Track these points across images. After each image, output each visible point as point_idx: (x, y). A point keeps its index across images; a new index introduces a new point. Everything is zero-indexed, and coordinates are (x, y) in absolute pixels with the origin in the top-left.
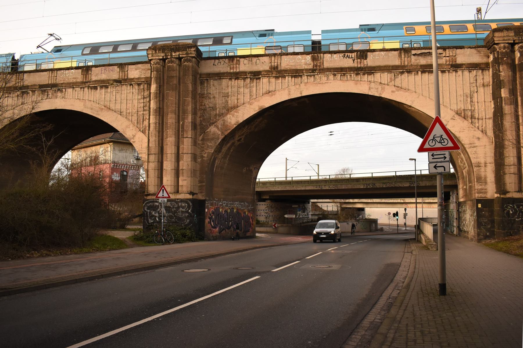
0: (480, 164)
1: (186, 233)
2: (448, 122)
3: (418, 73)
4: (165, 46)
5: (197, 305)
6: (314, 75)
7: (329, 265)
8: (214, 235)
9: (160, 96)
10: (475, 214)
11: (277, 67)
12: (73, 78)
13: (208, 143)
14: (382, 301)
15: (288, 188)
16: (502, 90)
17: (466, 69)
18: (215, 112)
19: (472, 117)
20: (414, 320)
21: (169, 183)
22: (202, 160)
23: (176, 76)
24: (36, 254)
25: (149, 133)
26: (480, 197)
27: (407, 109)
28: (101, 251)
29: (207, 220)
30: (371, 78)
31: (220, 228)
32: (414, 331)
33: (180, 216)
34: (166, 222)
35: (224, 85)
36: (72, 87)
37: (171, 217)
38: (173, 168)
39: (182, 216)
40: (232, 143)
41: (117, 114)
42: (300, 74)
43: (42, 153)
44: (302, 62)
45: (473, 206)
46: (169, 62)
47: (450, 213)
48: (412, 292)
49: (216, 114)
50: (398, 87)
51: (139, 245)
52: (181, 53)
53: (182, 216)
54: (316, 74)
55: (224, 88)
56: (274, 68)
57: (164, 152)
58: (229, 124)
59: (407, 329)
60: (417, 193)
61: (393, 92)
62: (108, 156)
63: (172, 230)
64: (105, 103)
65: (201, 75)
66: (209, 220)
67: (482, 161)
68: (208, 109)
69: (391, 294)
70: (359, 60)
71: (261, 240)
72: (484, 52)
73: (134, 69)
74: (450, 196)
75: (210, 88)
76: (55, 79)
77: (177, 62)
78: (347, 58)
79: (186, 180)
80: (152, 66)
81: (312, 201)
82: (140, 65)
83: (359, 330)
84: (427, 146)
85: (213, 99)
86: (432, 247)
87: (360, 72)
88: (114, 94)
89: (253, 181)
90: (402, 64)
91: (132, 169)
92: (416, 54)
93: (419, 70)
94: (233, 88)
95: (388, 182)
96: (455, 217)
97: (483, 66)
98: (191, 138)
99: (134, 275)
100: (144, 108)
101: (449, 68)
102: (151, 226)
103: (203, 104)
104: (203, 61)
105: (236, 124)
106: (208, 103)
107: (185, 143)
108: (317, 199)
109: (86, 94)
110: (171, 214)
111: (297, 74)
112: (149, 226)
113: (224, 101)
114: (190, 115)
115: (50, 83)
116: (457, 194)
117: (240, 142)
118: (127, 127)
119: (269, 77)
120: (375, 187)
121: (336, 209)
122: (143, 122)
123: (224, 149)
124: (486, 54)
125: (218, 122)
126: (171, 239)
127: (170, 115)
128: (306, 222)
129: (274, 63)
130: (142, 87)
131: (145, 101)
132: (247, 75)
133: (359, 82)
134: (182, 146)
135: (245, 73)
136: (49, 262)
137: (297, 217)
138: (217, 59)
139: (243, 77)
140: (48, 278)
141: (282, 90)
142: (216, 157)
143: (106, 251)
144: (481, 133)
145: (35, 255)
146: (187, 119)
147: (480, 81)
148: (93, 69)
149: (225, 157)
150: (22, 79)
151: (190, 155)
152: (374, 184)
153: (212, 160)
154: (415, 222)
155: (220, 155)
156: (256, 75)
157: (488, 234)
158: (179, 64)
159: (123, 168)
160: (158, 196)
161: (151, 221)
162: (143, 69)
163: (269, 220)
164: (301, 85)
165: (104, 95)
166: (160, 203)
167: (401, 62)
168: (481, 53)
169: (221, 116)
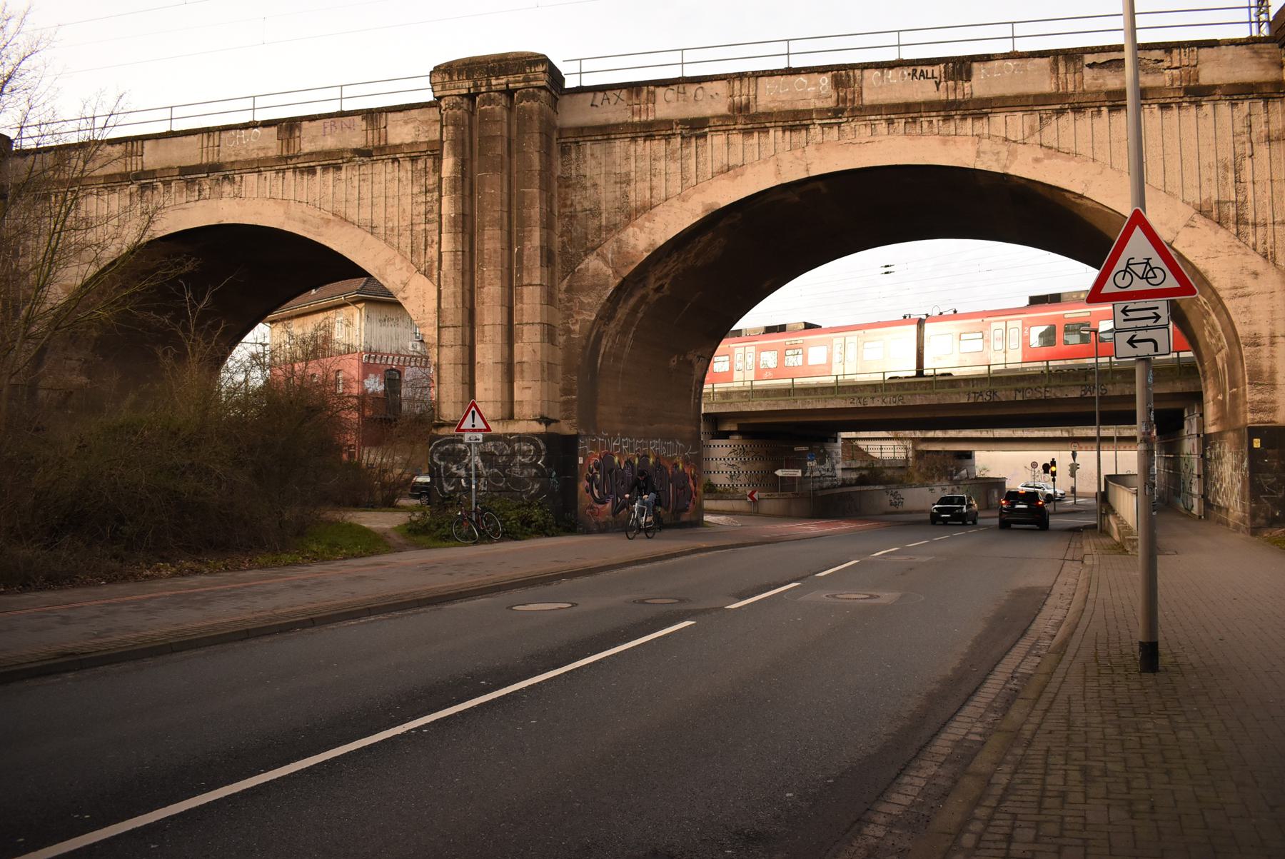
0: (1259, 338)
1: (531, 517)
2: (1178, 233)
3: (1099, 112)
4: (472, 64)
5: (525, 693)
6: (839, 124)
7: (869, 593)
8: (601, 519)
9: (463, 186)
10: (1245, 464)
11: (747, 106)
12: (258, 149)
13: (582, 298)
14: (994, 686)
15: (783, 405)
17: (1223, 98)
18: (597, 222)
19: (1240, 220)
20: (1068, 738)
21: (490, 396)
22: (569, 340)
23: (502, 136)
24: (168, 570)
25: (439, 274)
26: (1258, 422)
27: (1074, 203)
28: (325, 560)
29: (583, 485)
30: (981, 126)
31: (615, 504)
32: (1064, 767)
34: (484, 491)
35: (618, 155)
36: (257, 170)
37: (496, 478)
38: (500, 360)
39: (521, 474)
40: (639, 295)
41: (364, 233)
42: (805, 122)
43: (186, 329)
44: (808, 93)
45: (1241, 443)
46: (484, 102)
47: (1183, 464)
48: (1071, 663)
49: (600, 227)
50: (1050, 148)
51: (418, 546)
52: (511, 78)
53: (522, 473)
54: (845, 120)
55: (618, 161)
56: (741, 108)
57: (477, 321)
58: (631, 251)
59: (1046, 763)
60: (1101, 413)
61: (1037, 160)
62: (354, 337)
63: (498, 510)
64: (335, 205)
65: (561, 130)
66: (587, 484)
67: (1265, 331)
68: (580, 215)
69: (1018, 667)
70: (951, 83)
71: (715, 530)
72: (1269, 53)
73: (401, 123)
74: (1183, 419)
75: (585, 162)
76: (216, 152)
77: (503, 100)
78: (922, 78)
79: (529, 388)
80: (442, 112)
81: (844, 435)
82: (414, 113)
83: (922, 763)
84: (1109, 288)
85: (592, 191)
86: (1133, 548)
87: (953, 113)
88: (356, 184)
89: (696, 389)
90: (1061, 90)
91: (412, 364)
92: (1094, 63)
93: (1103, 103)
94: (639, 161)
96: (1196, 472)
97: (1267, 90)
98: (541, 285)
99: (390, 618)
100: (428, 216)
101: (1180, 98)
102: (449, 499)
103: (569, 202)
104: (566, 97)
105: (649, 250)
106: (580, 200)
107: (526, 300)
108: (857, 430)
109: (289, 185)
110: (496, 470)
111: (798, 122)
112: (444, 499)
113: (618, 194)
114: (538, 229)
115: (205, 161)
116: (1202, 415)
117: (661, 294)
118: (389, 262)
119: (727, 133)
120: (997, 400)
121: (903, 455)
122: (426, 249)
123: (622, 313)
124: (1274, 58)
125: (606, 245)
126: (496, 529)
127: (489, 232)
128: (828, 488)
129: (740, 96)
130: (421, 165)
131: (429, 199)
132: (674, 127)
133: (950, 137)
134: (519, 306)
135: (668, 123)
136: (195, 588)
137: (808, 474)
138: (601, 91)
139: (663, 133)
140: (180, 628)
141: (759, 164)
142: (601, 330)
143: (335, 560)
144: (1260, 259)
145: (164, 573)
146: (530, 241)
147: (1259, 128)
148: (305, 124)
149: (623, 332)
150: (139, 154)
151: (538, 327)
153: (592, 338)
154: (1096, 486)
155: (612, 327)
156: (696, 128)
157: (1278, 514)
158: (509, 106)
159: (390, 362)
161: (448, 488)
162: (422, 122)
163: (739, 483)
164: (806, 149)
165: (331, 188)
166: (469, 445)
167: (1058, 85)
168: (1262, 57)
169: (611, 230)
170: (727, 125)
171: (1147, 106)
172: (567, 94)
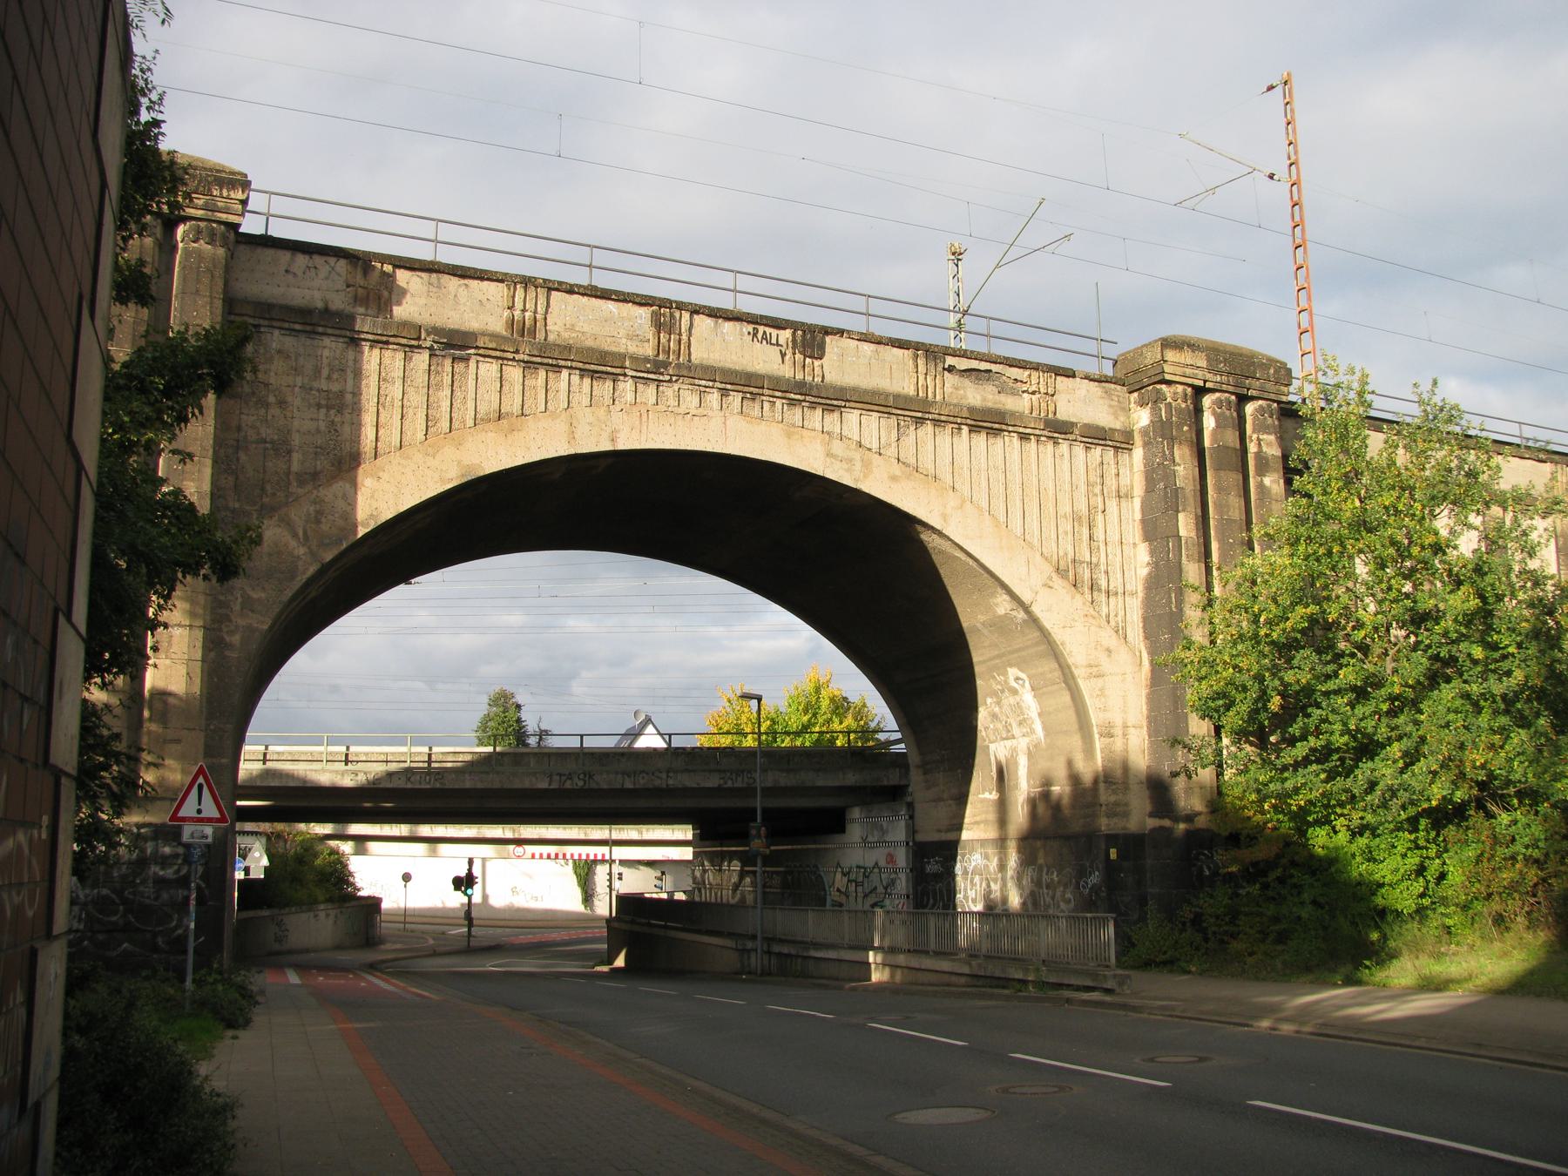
16: (1181, 516)
17: (1080, 439)
30: (832, 420)
33: (147, 901)
39: (156, 899)
61: (894, 478)
78: (764, 342)
93: (964, 421)
95: (643, 771)
110: (105, 891)
119: (500, 361)
120: (594, 786)
133: (796, 429)
152: (590, 777)
160: (182, 813)
164: (611, 407)
170: (504, 351)
171: (1006, 433)
172: (245, 243)
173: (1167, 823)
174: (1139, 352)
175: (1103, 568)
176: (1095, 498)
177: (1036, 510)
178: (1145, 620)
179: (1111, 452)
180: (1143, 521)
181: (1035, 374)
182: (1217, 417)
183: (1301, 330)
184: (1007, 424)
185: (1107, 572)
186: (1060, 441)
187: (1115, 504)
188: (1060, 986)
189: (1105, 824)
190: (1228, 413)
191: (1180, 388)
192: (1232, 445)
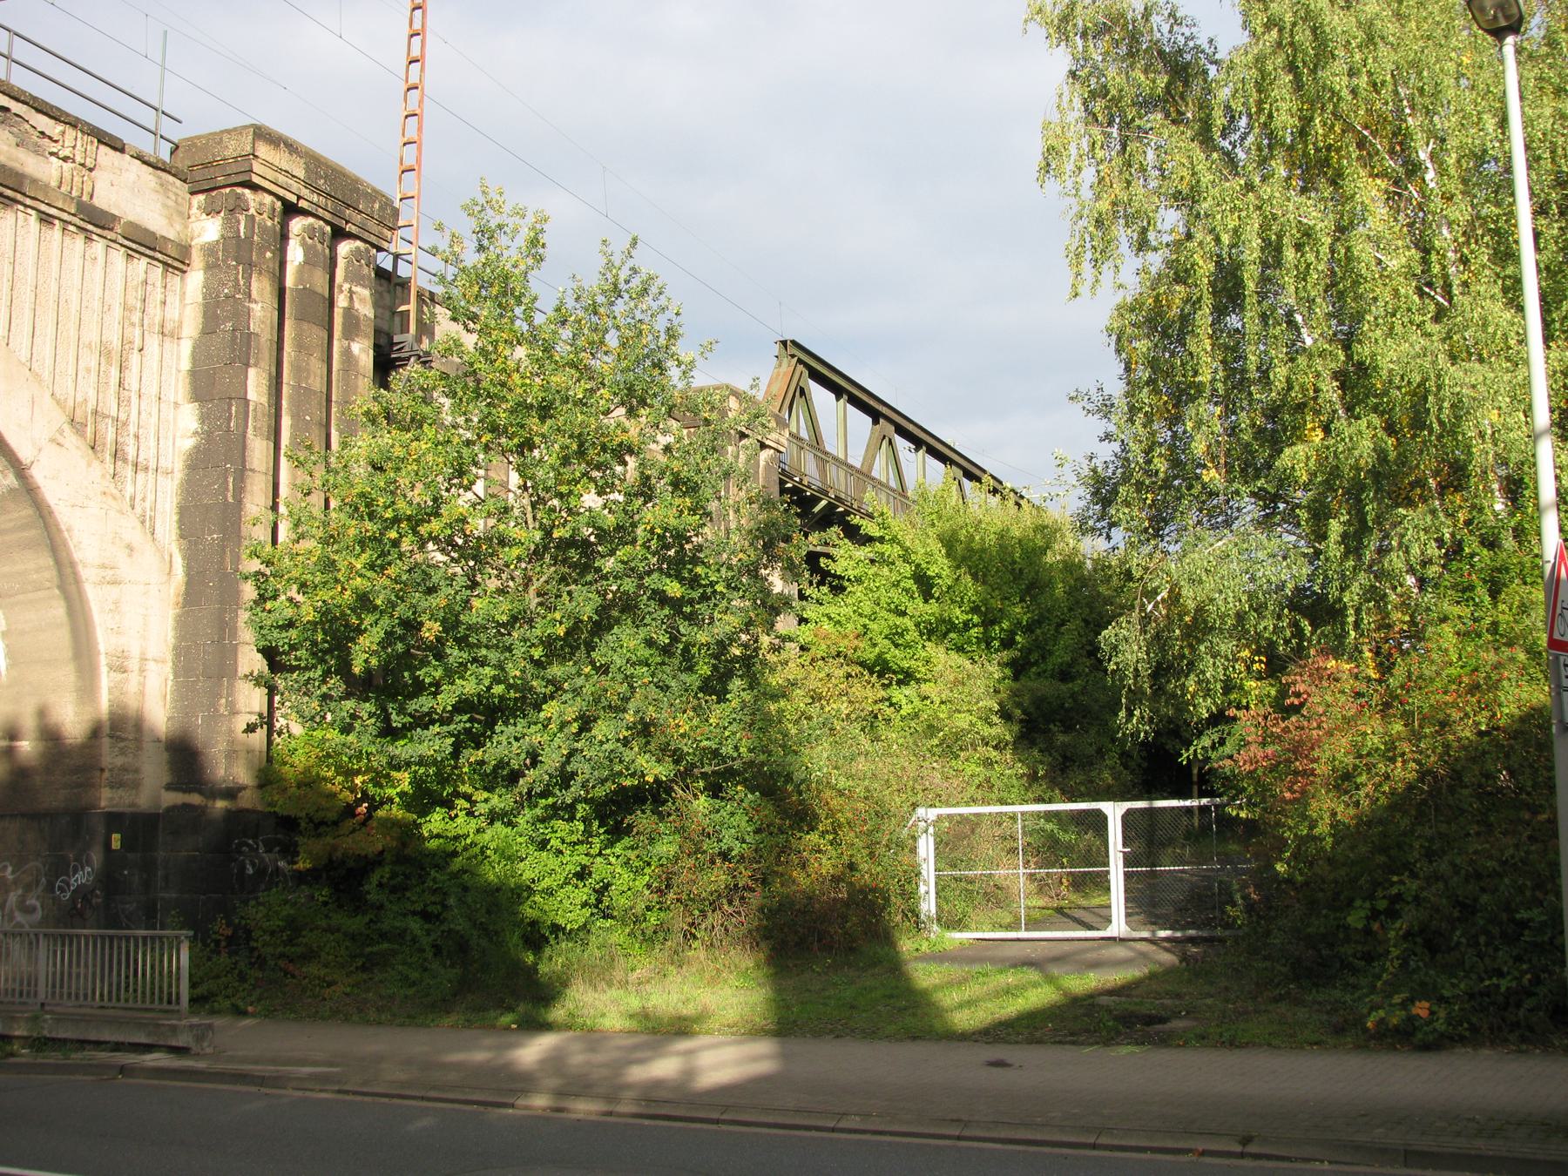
16: (252, 372)
17: (121, 240)
171: (21, 207)
173: (195, 799)
174: (217, 138)
175: (132, 429)
176: (130, 329)
177: (51, 329)
178: (183, 512)
179: (160, 269)
180: (194, 374)
181: (71, 133)
182: (308, 250)
183: (404, 168)
184: (24, 194)
185: (137, 437)
186: (95, 237)
187: (156, 342)
188: (82, 1044)
189: (107, 799)
190: (319, 246)
191: (268, 199)
192: (320, 290)
